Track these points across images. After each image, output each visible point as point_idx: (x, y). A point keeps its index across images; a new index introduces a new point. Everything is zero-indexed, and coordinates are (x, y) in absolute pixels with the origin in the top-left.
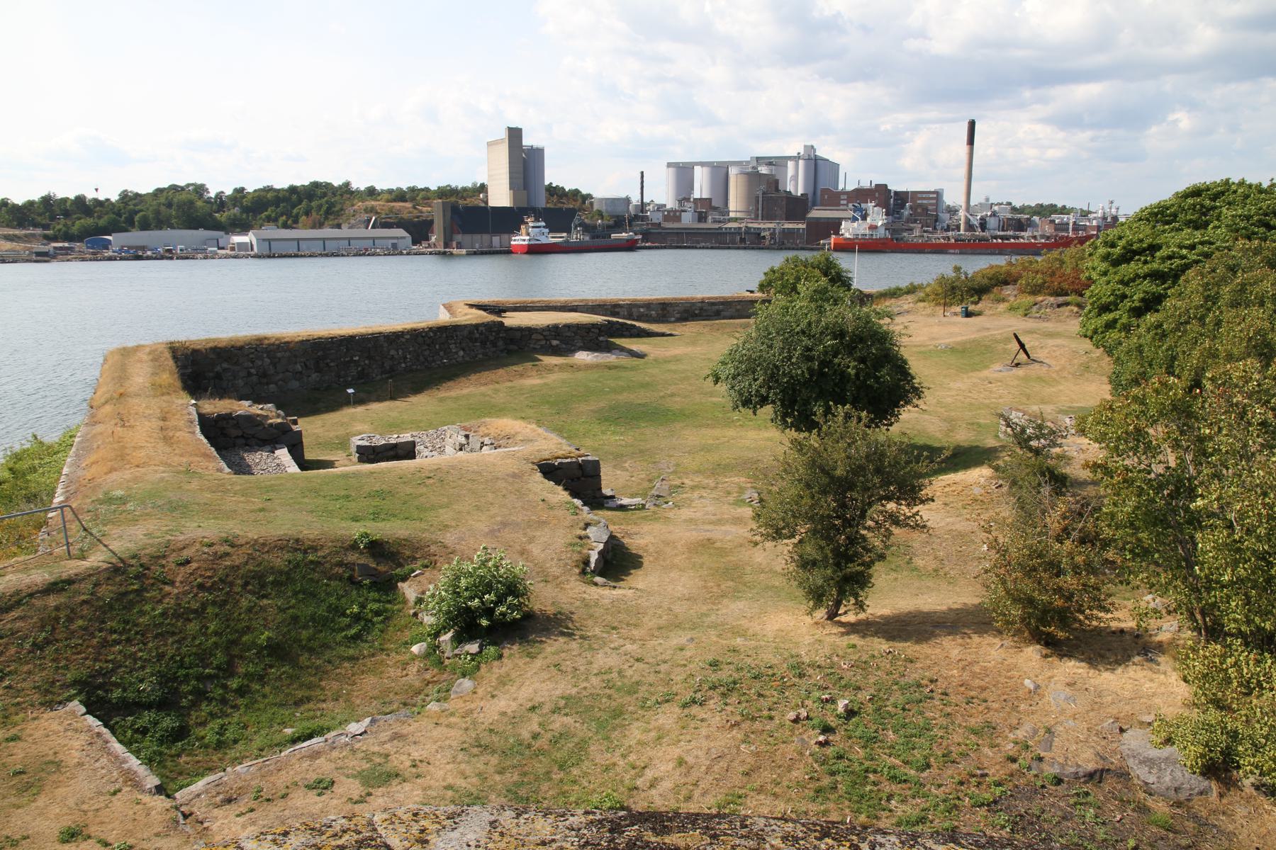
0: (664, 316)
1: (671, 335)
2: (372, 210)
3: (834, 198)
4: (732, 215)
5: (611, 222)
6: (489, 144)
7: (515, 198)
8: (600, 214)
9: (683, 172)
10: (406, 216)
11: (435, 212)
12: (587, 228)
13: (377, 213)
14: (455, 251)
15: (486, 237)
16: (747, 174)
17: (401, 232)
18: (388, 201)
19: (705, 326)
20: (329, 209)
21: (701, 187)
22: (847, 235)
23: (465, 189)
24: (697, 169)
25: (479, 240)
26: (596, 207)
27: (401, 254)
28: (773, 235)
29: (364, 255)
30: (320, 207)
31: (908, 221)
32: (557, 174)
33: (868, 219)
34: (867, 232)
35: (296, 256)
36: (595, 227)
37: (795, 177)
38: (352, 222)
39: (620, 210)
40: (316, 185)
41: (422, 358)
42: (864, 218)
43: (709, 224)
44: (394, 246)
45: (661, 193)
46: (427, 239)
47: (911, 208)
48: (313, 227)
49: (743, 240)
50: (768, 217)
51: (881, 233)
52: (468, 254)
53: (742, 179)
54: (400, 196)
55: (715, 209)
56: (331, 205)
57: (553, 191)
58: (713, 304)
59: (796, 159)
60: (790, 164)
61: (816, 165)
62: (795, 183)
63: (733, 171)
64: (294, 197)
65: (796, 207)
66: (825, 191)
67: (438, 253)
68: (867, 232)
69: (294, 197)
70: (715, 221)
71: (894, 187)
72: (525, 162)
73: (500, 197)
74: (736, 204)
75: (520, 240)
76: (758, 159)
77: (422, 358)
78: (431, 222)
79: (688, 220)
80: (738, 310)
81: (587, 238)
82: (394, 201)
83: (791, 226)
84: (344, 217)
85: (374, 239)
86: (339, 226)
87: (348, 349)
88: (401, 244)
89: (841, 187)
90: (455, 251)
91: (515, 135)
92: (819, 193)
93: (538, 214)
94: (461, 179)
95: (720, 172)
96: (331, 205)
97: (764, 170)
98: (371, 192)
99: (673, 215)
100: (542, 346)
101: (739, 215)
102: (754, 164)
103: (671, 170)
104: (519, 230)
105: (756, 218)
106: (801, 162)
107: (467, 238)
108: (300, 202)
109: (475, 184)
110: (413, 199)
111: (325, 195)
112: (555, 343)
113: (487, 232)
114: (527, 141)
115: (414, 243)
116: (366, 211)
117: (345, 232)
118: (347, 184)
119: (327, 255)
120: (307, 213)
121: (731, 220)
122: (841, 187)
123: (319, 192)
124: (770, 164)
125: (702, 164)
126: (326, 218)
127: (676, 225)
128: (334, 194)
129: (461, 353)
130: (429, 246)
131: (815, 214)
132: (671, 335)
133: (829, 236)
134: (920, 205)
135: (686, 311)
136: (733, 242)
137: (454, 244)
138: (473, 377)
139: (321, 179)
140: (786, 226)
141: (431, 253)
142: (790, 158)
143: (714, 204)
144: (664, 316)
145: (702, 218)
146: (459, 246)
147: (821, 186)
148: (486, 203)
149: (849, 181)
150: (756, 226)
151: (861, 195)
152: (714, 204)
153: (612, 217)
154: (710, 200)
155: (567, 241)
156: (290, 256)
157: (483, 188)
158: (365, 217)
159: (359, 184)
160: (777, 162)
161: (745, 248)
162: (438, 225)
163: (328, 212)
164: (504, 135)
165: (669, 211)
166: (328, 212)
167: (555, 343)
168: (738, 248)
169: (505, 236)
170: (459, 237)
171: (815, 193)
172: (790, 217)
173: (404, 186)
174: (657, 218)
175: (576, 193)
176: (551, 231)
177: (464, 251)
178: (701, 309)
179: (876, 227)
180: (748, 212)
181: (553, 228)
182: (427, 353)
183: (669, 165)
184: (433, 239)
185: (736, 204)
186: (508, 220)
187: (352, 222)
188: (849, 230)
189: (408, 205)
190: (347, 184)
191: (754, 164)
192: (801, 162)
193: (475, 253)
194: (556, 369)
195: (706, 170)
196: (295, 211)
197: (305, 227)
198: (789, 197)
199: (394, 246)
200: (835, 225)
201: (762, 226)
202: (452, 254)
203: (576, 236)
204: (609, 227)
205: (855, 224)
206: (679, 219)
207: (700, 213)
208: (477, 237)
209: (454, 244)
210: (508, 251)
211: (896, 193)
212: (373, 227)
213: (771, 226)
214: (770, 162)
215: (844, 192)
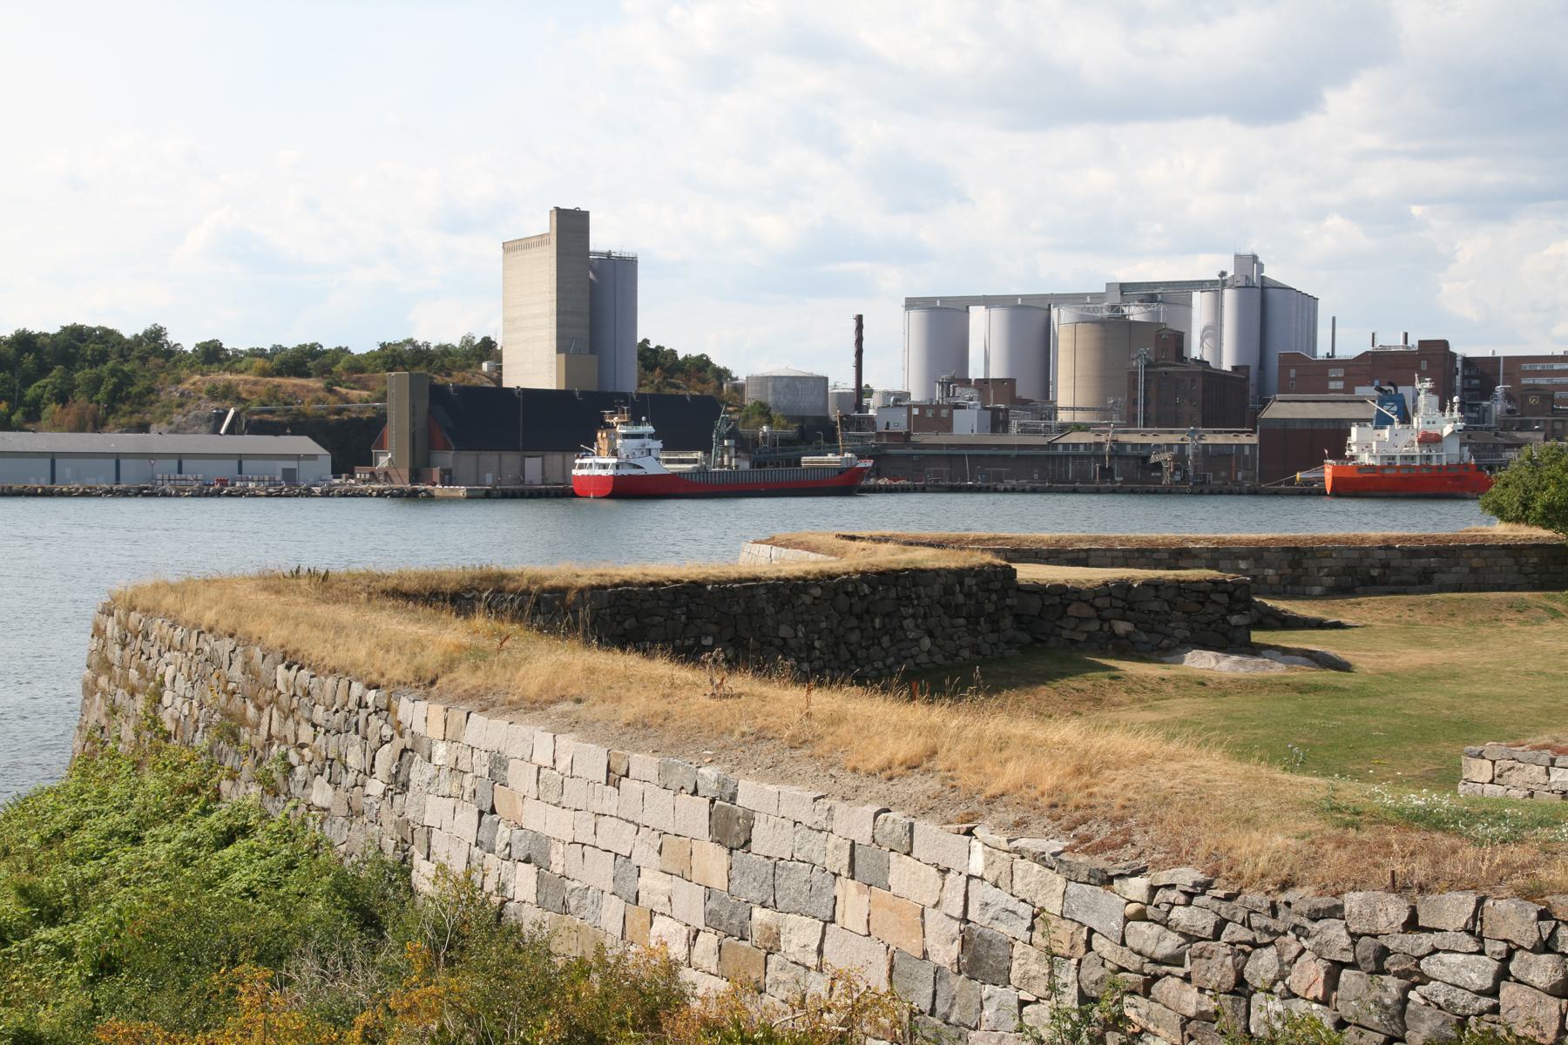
0: (1296, 581)
1: (1338, 626)
2: (227, 393)
3: (1312, 375)
4: (1064, 417)
5: (791, 431)
6: (509, 247)
7: (570, 370)
8: (764, 411)
9: (944, 320)
10: (310, 408)
11: (397, 392)
12: (745, 445)
13: (239, 400)
14: (438, 490)
15: (510, 459)
16: (1102, 322)
17: (304, 444)
18: (265, 373)
19: (1412, 607)
20: (118, 388)
21: (987, 349)
22: (1365, 459)
23: (445, 351)
24: (977, 315)
25: (495, 465)
26: (750, 397)
27: (308, 493)
28: (1180, 458)
29: (218, 494)
30: (97, 383)
31: (1506, 426)
32: (665, 321)
33: (1417, 421)
34: (1417, 450)
35: (48, 494)
36: (755, 441)
37: (1214, 331)
38: (178, 418)
39: (807, 404)
40: (76, 335)
41: (843, 651)
42: (1406, 419)
43: (1014, 437)
44: (289, 475)
45: (897, 370)
46: (368, 461)
47: (1508, 396)
48: (81, 428)
49: (1107, 473)
50: (1161, 418)
51: (1452, 453)
52: (472, 497)
53: (1086, 334)
54: (303, 361)
55: (1024, 403)
56: (126, 379)
57: (655, 360)
58: (1414, 553)
59: (1215, 287)
60: (1200, 301)
61: (1266, 303)
62: (1214, 337)
63: (1062, 318)
64: (29, 360)
65: (1225, 396)
66: (1289, 360)
67: (400, 495)
68: (1417, 450)
69: (29, 360)
70: (1025, 430)
71: (1464, 348)
72: (594, 289)
73: (533, 365)
74: (1071, 388)
75: (595, 465)
76: (1124, 288)
77: (843, 651)
78: (379, 422)
79: (967, 425)
80: (1474, 570)
81: (746, 465)
82: (279, 373)
83: (1220, 439)
84: (158, 409)
85: (240, 458)
86: (144, 428)
87: (691, 617)
88: (306, 473)
89: (1322, 351)
90: (438, 490)
91: (572, 225)
92: (1274, 364)
93: (638, 409)
94: (440, 328)
95: (1031, 319)
96: (126, 379)
97: (1136, 313)
98: (212, 354)
99: (934, 416)
100: (1091, 637)
101: (1080, 417)
102: (1116, 299)
103: (915, 315)
104: (591, 440)
105: (1132, 421)
106: (1229, 295)
107: (464, 461)
108: (44, 370)
109: (468, 341)
110: (325, 371)
111: (102, 357)
112: (1122, 627)
113: (514, 448)
114: (601, 240)
115: (336, 472)
116: (213, 394)
117: (157, 440)
118: (156, 335)
119: (125, 494)
120: (63, 398)
121: (1064, 428)
122: (1322, 351)
123: (89, 350)
124: (1152, 299)
125: (988, 301)
126: (111, 410)
127: (943, 439)
128: (124, 357)
129: (926, 643)
130: (374, 477)
131: (1279, 410)
132: (1338, 626)
133: (1318, 462)
134: (1535, 389)
135: (1349, 570)
136: (1085, 479)
137: (436, 473)
138: (1010, 696)
139: (90, 321)
140: (1210, 439)
141: (380, 494)
142: (1200, 285)
143: (1021, 392)
144: (1296, 581)
145: (998, 423)
146: (448, 478)
147: (1278, 348)
148: (499, 380)
149: (1344, 334)
150: (1136, 439)
151: (1387, 371)
152: (1021, 392)
153: (791, 419)
154: (1010, 382)
155: (703, 471)
156: (33, 494)
157: (487, 349)
158: (213, 407)
159: (185, 338)
160: (1172, 295)
161: (1114, 491)
162: (398, 429)
163: (116, 397)
164: (544, 224)
165: (922, 407)
166: (116, 397)
167: (1122, 627)
168: (1098, 491)
169: (555, 459)
170: (447, 458)
171: (1262, 365)
172: (1213, 418)
173: (291, 341)
174: (899, 421)
175: (702, 364)
176: (665, 449)
177: (461, 491)
178: (1385, 566)
179: (1437, 439)
180: (1103, 410)
181: (673, 441)
182: (855, 637)
183: (911, 304)
184: (383, 461)
185: (1071, 388)
186: (562, 419)
187: (178, 418)
188: (1368, 446)
189: (314, 383)
190: (156, 335)
191: (1116, 299)
192: (1229, 295)
193: (488, 495)
194: (1169, 688)
195: (998, 314)
196: (31, 392)
197: (56, 427)
198: (1207, 374)
199: (289, 475)
200: (1333, 437)
201: (1150, 439)
202: (430, 497)
203: (727, 460)
204: (786, 441)
205: (1386, 433)
206: (947, 425)
207: (995, 411)
208: (490, 458)
209: (436, 473)
210: (563, 492)
211: (1468, 362)
212: (231, 430)
213: (1174, 439)
214: (1150, 294)
215: (1331, 362)
